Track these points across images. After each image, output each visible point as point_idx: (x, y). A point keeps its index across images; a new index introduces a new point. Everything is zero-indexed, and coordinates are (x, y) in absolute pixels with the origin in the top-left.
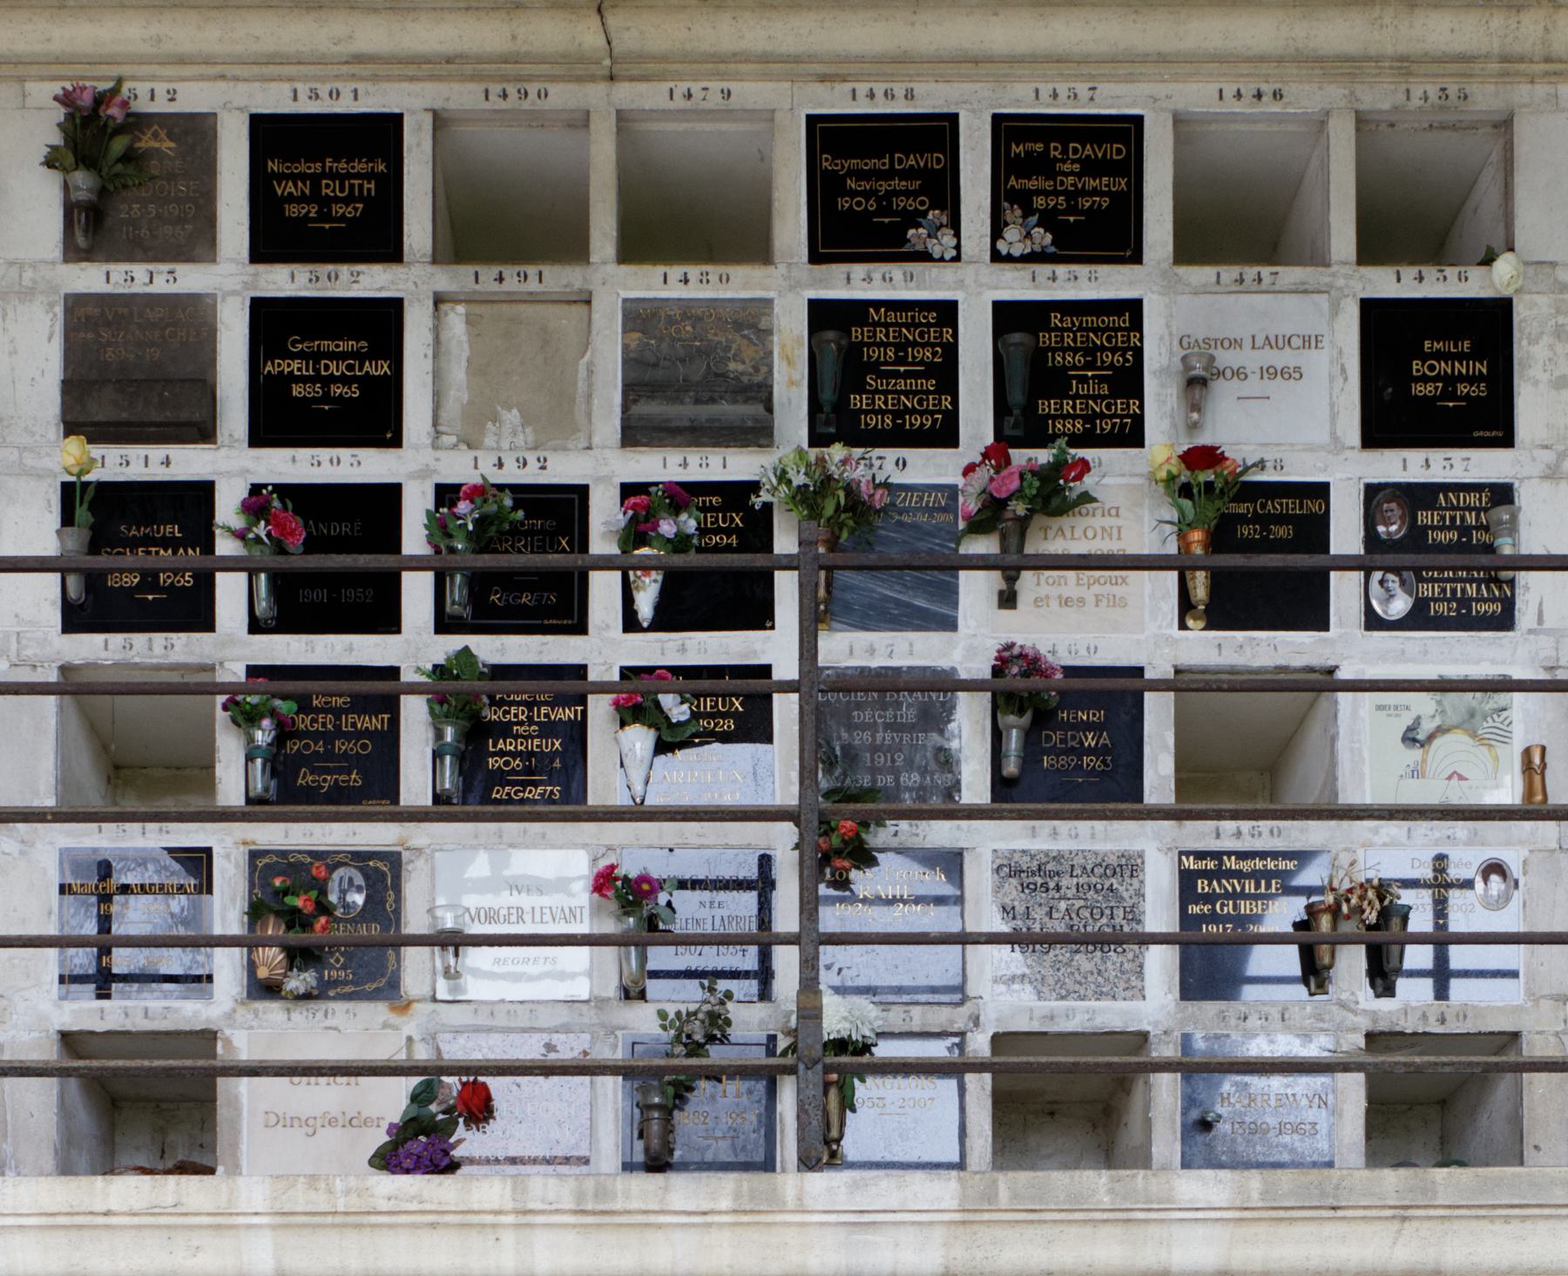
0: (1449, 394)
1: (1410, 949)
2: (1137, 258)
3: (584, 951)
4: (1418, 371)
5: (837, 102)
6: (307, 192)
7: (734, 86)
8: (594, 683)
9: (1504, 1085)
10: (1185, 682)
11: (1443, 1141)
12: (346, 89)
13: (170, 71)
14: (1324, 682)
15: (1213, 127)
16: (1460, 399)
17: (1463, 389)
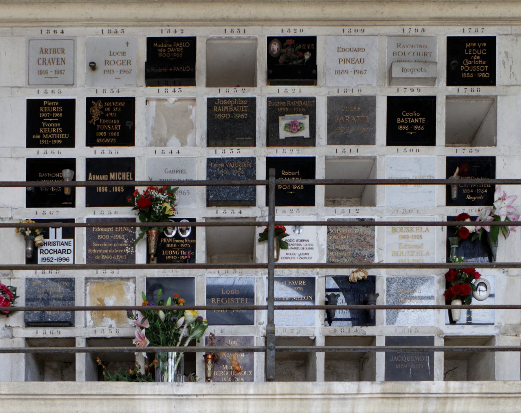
1: (337, 311)
4: (399, 121)
7: (426, 28)
8: (77, 224)
9: (489, 354)
10: (208, 224)
11: (468, 371)
13: (238, 23)
14: (371, 223)
16: (415, 131)
17: (416, 127)
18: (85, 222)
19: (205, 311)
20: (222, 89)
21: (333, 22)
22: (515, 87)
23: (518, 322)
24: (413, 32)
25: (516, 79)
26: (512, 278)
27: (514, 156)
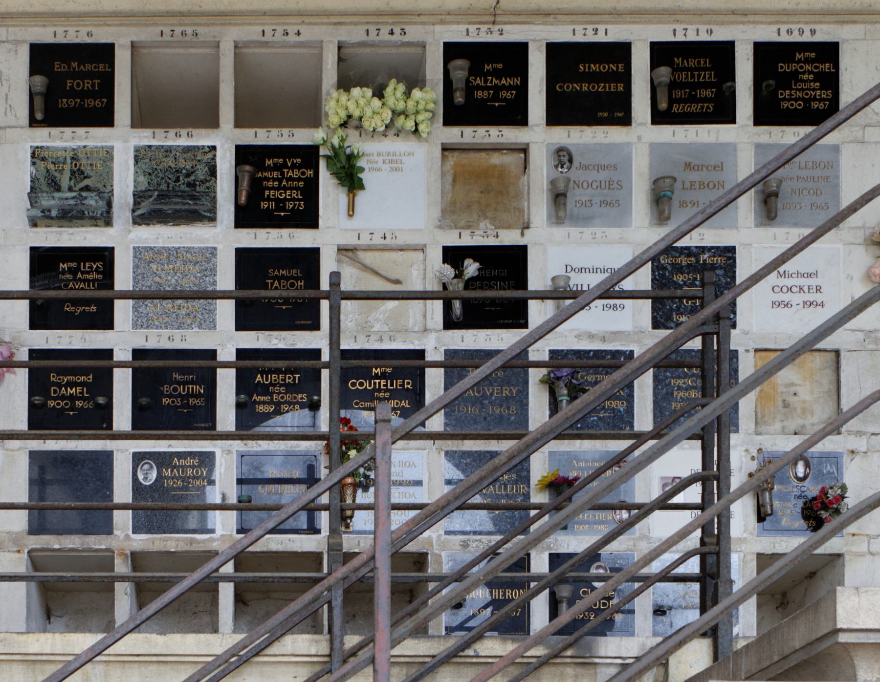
0: (495, 98)
2: (732, 120)
3: (61, 511)
5: (46, 35)
6: (519, 83)
12: (601, 28)
15: (154, 50)
16: (78, 409)
18: (547, 358)
19: (131, 511)
20: (157, 131)
21: (386, 17)
22: (14, 130)
23: (21, 529)
24: (279, 37)
25: (15, 116)
26: (11, 453)
27: (14, 246)
